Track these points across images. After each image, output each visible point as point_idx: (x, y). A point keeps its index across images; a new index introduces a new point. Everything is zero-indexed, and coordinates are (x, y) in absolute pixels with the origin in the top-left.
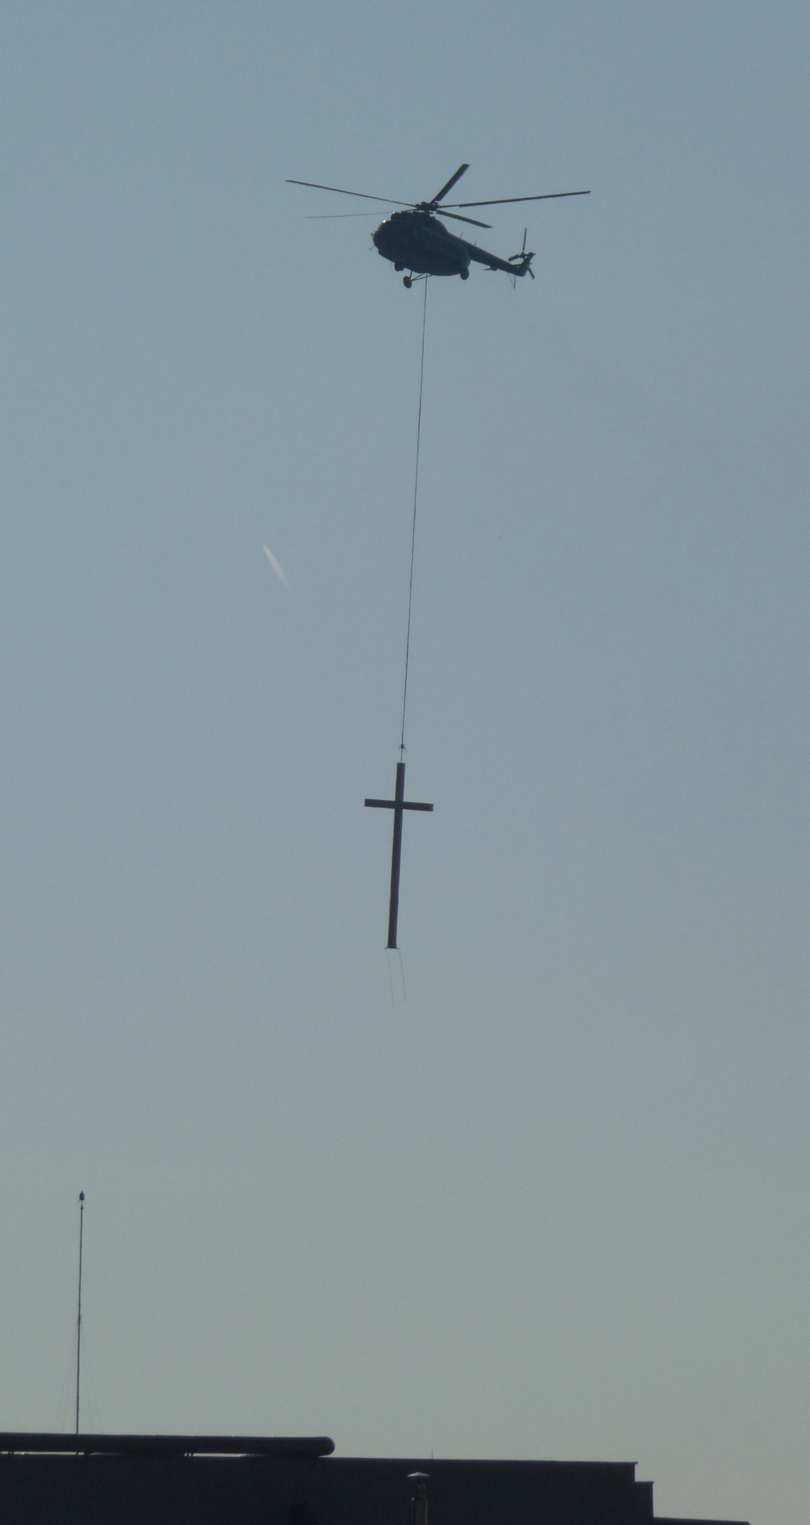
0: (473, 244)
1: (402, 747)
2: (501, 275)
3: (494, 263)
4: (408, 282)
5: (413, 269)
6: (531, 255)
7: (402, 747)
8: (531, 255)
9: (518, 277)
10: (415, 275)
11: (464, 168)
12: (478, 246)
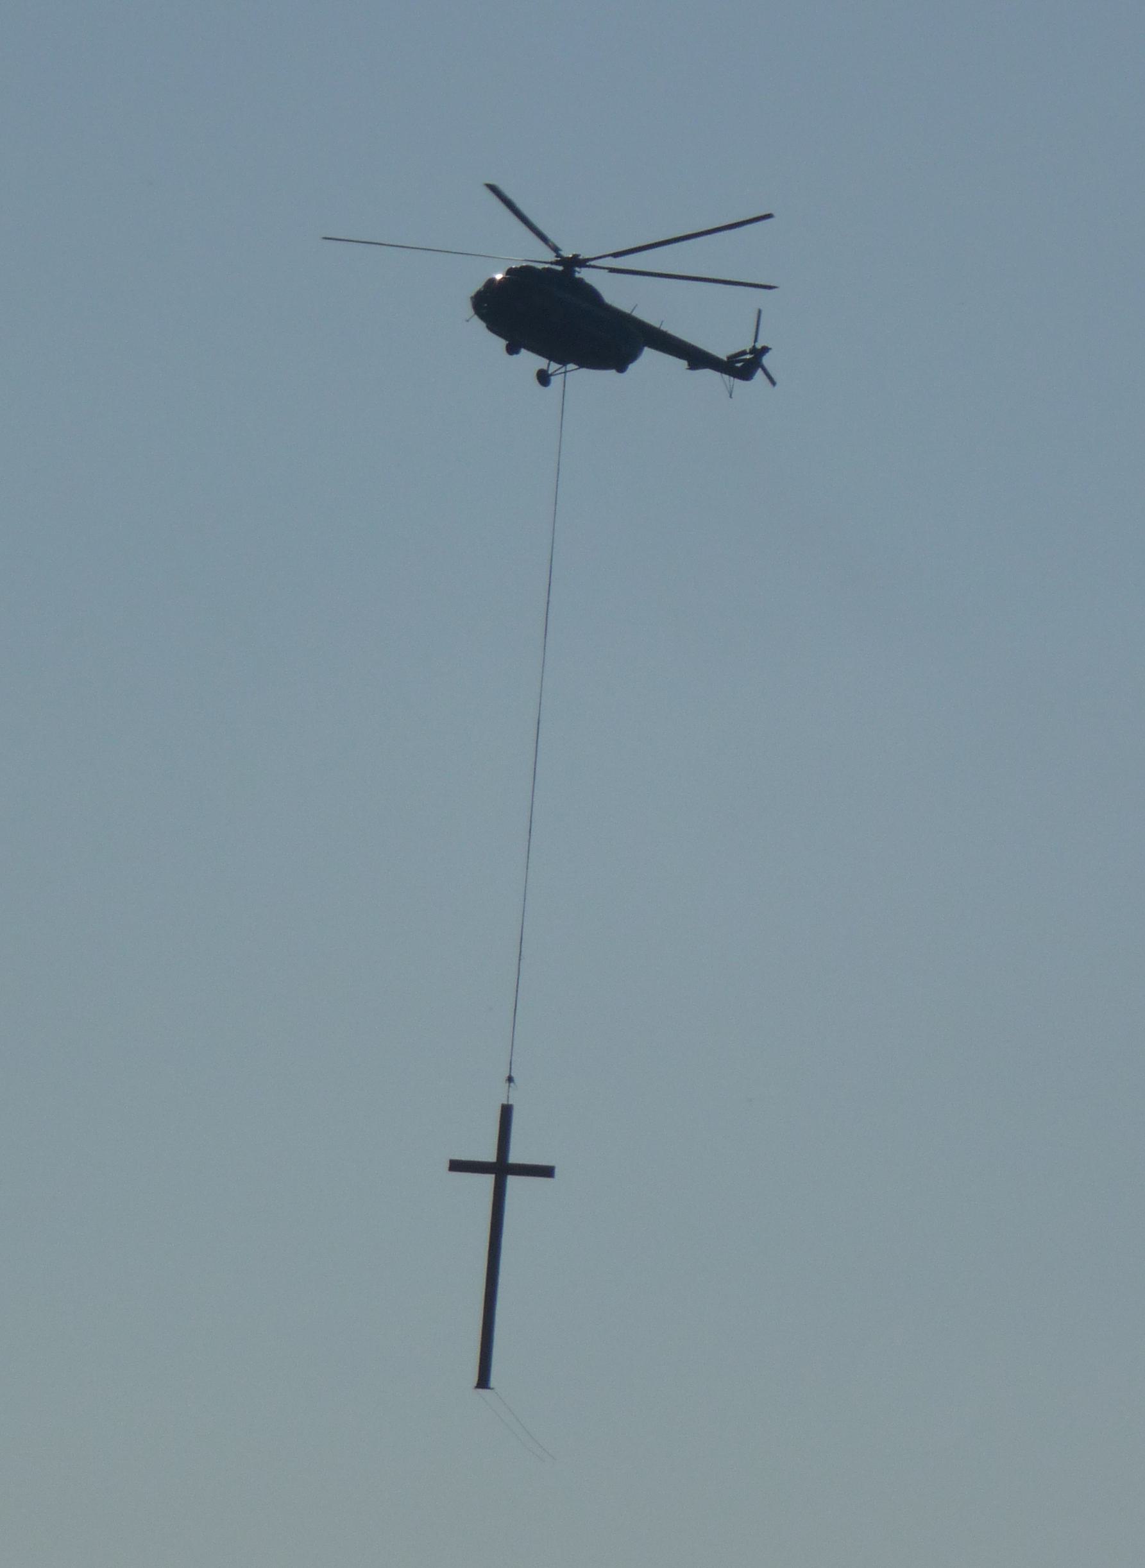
0: (657, 325)
1: (510, 1079)
2: (708, 375)
3: (697, 359)
4: (544, 378)
5: (551, 357)
6: (765, 350)
7: (510, 1079)
8: (765, 350)
9: (738, 383)
10: (554, 366)
11: (769, 216)
12: (664, 328)
